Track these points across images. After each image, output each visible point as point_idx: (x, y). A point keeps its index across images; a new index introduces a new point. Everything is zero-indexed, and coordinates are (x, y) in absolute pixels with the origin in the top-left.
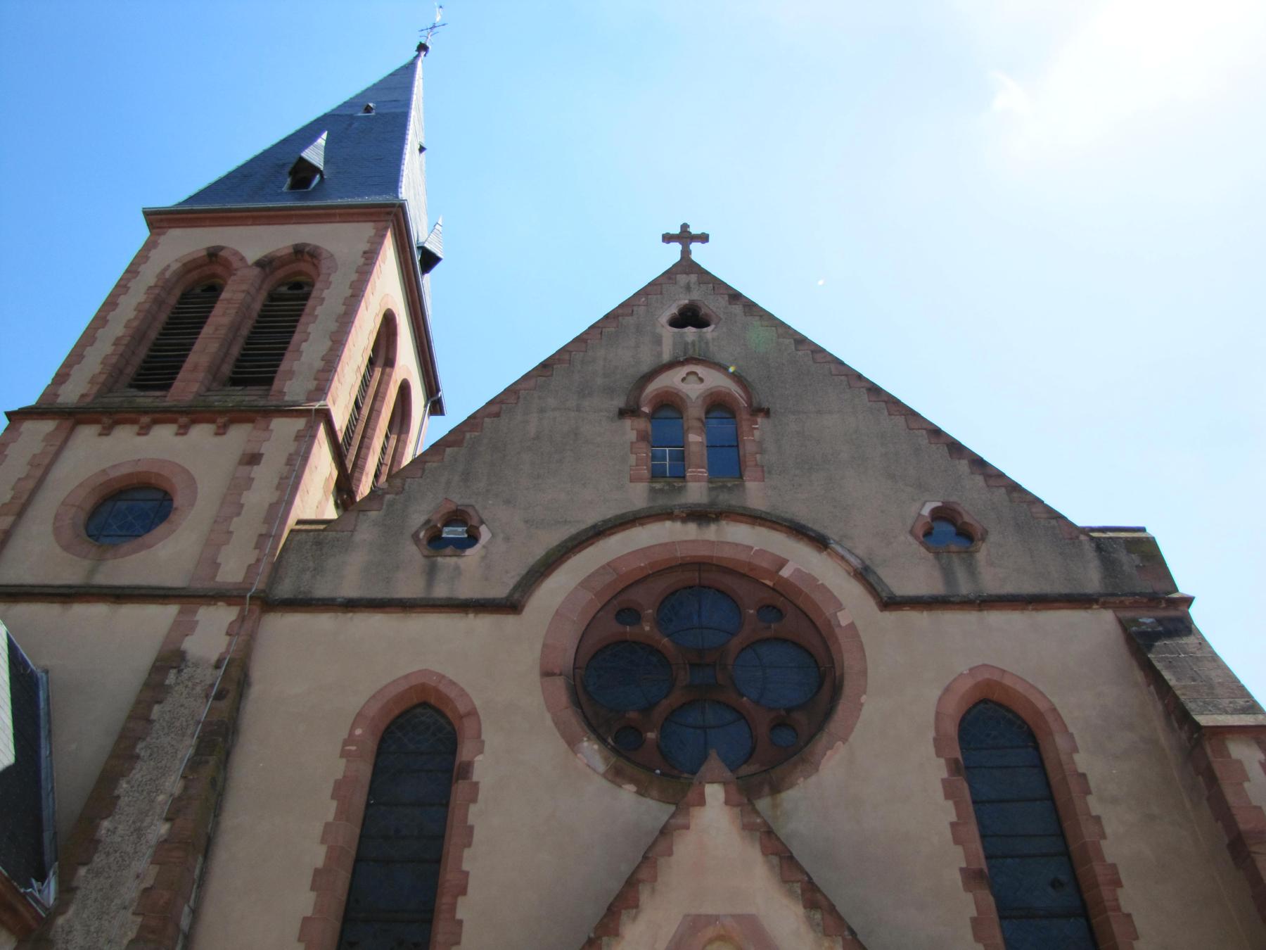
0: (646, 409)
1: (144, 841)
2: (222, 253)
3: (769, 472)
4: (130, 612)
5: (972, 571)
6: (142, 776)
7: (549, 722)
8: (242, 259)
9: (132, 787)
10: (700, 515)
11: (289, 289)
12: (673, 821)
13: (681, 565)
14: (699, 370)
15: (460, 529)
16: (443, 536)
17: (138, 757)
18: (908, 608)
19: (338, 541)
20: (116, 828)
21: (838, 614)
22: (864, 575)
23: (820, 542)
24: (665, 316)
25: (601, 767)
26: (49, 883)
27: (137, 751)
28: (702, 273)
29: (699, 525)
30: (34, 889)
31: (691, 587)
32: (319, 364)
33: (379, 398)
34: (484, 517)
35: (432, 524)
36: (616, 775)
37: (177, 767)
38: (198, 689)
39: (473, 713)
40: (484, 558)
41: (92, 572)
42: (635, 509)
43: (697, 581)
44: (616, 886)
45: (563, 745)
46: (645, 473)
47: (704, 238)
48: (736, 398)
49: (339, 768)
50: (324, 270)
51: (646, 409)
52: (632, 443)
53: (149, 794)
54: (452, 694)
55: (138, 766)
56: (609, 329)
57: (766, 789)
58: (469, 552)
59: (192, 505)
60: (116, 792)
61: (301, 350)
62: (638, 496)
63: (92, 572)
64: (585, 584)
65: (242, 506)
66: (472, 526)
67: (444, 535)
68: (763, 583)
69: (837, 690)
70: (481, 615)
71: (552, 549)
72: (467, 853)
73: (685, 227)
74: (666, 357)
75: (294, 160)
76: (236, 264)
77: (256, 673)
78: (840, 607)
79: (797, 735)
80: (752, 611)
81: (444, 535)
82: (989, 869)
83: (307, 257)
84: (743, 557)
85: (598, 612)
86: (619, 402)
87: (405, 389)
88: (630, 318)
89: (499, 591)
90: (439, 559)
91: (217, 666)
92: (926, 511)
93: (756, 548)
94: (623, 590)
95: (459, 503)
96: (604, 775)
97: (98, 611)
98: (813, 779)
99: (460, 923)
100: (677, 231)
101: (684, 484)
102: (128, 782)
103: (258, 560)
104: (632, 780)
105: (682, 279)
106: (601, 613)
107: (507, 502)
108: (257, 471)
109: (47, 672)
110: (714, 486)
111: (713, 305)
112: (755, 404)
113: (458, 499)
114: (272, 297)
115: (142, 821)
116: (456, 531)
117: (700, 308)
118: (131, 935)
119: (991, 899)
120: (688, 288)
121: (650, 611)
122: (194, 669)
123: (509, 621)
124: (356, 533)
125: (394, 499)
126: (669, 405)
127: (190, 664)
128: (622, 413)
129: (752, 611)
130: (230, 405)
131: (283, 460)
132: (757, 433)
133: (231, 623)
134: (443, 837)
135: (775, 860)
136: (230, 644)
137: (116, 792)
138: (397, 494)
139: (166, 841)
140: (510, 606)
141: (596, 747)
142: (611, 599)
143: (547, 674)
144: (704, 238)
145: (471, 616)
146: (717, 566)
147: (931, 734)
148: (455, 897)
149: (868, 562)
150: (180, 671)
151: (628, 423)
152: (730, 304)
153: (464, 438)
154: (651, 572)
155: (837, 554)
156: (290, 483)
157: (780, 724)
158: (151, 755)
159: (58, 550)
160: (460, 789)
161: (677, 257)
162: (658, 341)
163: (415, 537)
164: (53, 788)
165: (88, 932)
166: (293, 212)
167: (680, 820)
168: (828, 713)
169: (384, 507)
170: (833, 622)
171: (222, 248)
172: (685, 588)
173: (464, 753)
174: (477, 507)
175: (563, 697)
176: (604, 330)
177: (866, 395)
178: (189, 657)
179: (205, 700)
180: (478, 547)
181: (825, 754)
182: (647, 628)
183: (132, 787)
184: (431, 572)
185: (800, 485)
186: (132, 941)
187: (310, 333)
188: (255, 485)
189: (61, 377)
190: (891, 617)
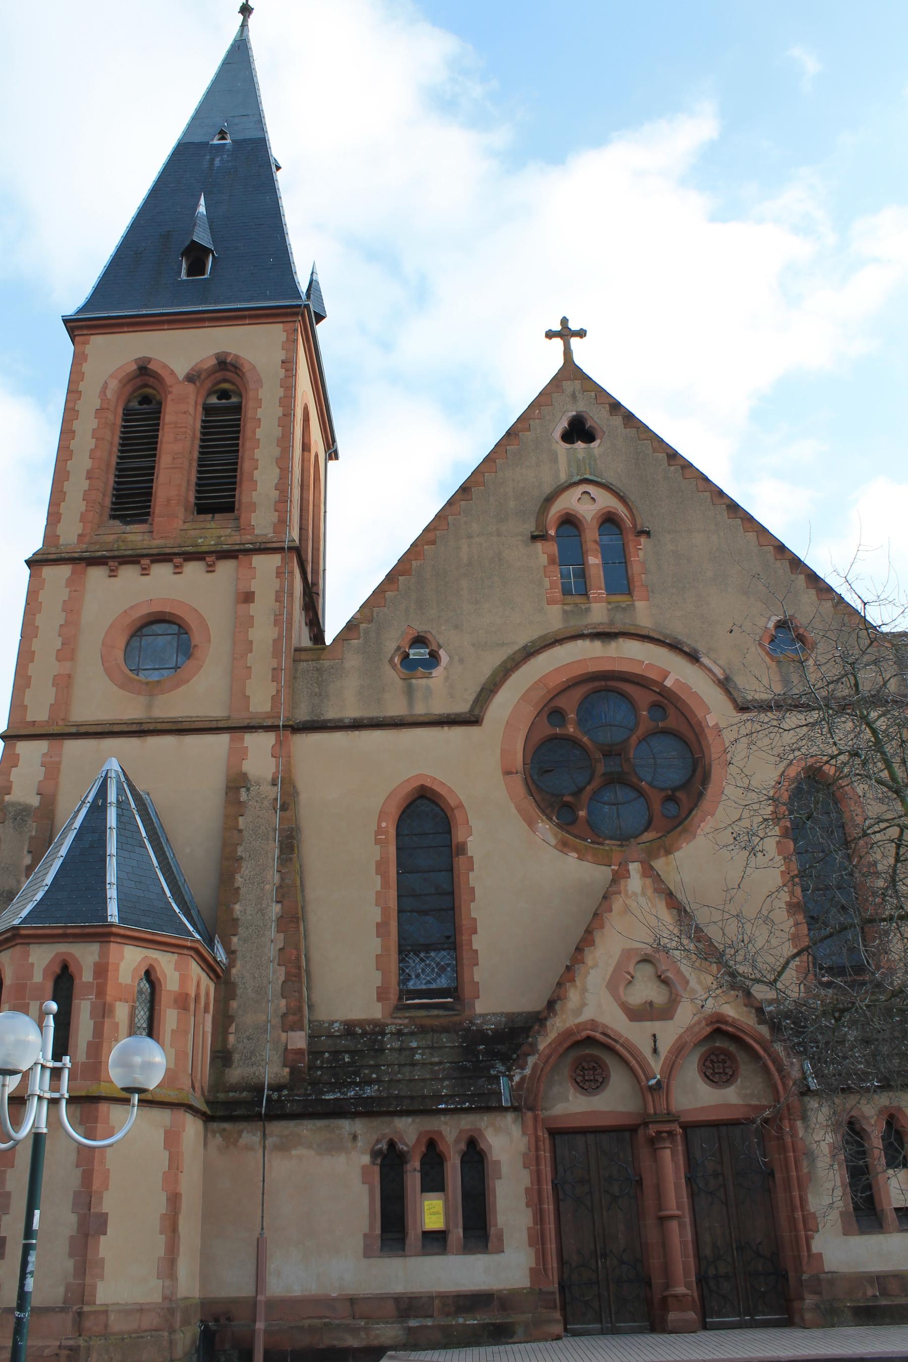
0: (552, 532)
1: (267, 918)
2: (149, 366)
3: (653, 592)
4: (191, 740)
6: (250, 872)
7: (514, 811)
8: (172, 373)
9: (246, 880)
11: (219, 398)
12: (610, 889)
14: (590, 488)
15: (422, 651)
17: (241, 858)
19: (332, 668)
20: (245, 910)
21: (707, 716)
22: (725, 684)
23: (693, 657)
24: (557, 434)
25: (553, 842)
26: (217, 948)
27: (239, 854)
28: (584, 379)
29: (603, 642)
30: (762, 1160)
32: (275, 494)
33: (305, 487)
34: (441, 642)
35: (402, 650)
36: (564, 846)
37: (271, 864)
38: (266, 803)
39: (460, 806)
40: (447, 678)
41: (149, 706)
42: (554, 630)
44: (580, 932)
45: (527, 827)
46: (558, 593)
47: (581, 334)
48: (623, 520)
49: (376, 852)
50: (251, 385)
51: (552, 532)
52: (545, 567)
53: (258, 884)
54: (443, 792)
55: (244, 864)
56: (512, 447)
57: (662, 852)
59: (209, 641)
60: (236, 885)
61: (254, 479)
63: (149, 706)
64: (525, 698)
65: (251, 642)
66: (432, 650)
69: (706, 778)
71: (496, 668)
72: (473, 905)
73: (564, 321)
74: (563, 477)
75: (187, 243)
76: (168, 380)
77: (301, 785)
78: (708, 711)
81: (411, 657)
82: (803, 897)
83: (233, 369)
84: (637, 670)
85: (535, 718)
86: (530, 527)
87: (317, 456)
88: (529, 433)
89: (462, 707)
90: (414, 681)
91: (274, 784)
92: (771, 625)
93: (646, 662)
94: (551, 699)
95: (419, 630)
96: (555, 847)
97: (169, 741)
98: (692, 844)
99: (476, 951)
100: (557, 327)
101: (588, 605)
102: (241, 877)
103: (278, 691)
104: (575, 850)
105: (569, 386)
106: (537, 718)
107: (456, 627)
108: (253, 609)
109: (148, 794)
111: (597, 417)
112: (639, 528)
113: (419, 627)
114: (208, 410)
115: (261, 904)
117: (586, 419)
118: (282, 978)
121: (572, 716)
122: (258, 787)
123: (473, 730)
124: (345, 661)
125: (368, 628)
126: (569, 521)
127: (253, 783)
128: (534, 538)
129: (644, 713)
130: (213, 543)
131: (273, 597)
132: (641, 553)
133: (273, 747)
135: (675, 912)
136: (277, 765)
137: (236, 885)
138: (369, 623)
139: (282, 916)
140: (471, 720)
141: (547, 826)
143: (507, 773)
144: (581, 334)
145: (446, 728)
148: (470, 935)
149: (728, 671)
150: (248, 790)
151: (539, 545)
152: (611, 415)
153: (411, 565)
155: (705, 667)
157: (671, 798)
158: (250, 856)
159: (115, 688)
160: (460, 862)
161: (559, 362)
162: (554, 459)
163: (391, 661)
164: (185, 880)
165: (255, 977)
166: (206, 315)
167: (613, 889)
168: (700, 795)
169: (362, 635)
170: (704, 724)
171: (149, 360)
172: (594, 692)
173: (459, 835)
174: (433, 632)
175: (521, 789)
176: (508, 447)
177: (726, 513)
178: (250, 777)
179: (273, 811)
181: (699, 826)
182: (571, 730)
183: (246, 880)
184: (410, 692)
185: (677, 603)
186: (284, 982)
187: (258, 460)
188: (256, 622)
189: (54, 517)
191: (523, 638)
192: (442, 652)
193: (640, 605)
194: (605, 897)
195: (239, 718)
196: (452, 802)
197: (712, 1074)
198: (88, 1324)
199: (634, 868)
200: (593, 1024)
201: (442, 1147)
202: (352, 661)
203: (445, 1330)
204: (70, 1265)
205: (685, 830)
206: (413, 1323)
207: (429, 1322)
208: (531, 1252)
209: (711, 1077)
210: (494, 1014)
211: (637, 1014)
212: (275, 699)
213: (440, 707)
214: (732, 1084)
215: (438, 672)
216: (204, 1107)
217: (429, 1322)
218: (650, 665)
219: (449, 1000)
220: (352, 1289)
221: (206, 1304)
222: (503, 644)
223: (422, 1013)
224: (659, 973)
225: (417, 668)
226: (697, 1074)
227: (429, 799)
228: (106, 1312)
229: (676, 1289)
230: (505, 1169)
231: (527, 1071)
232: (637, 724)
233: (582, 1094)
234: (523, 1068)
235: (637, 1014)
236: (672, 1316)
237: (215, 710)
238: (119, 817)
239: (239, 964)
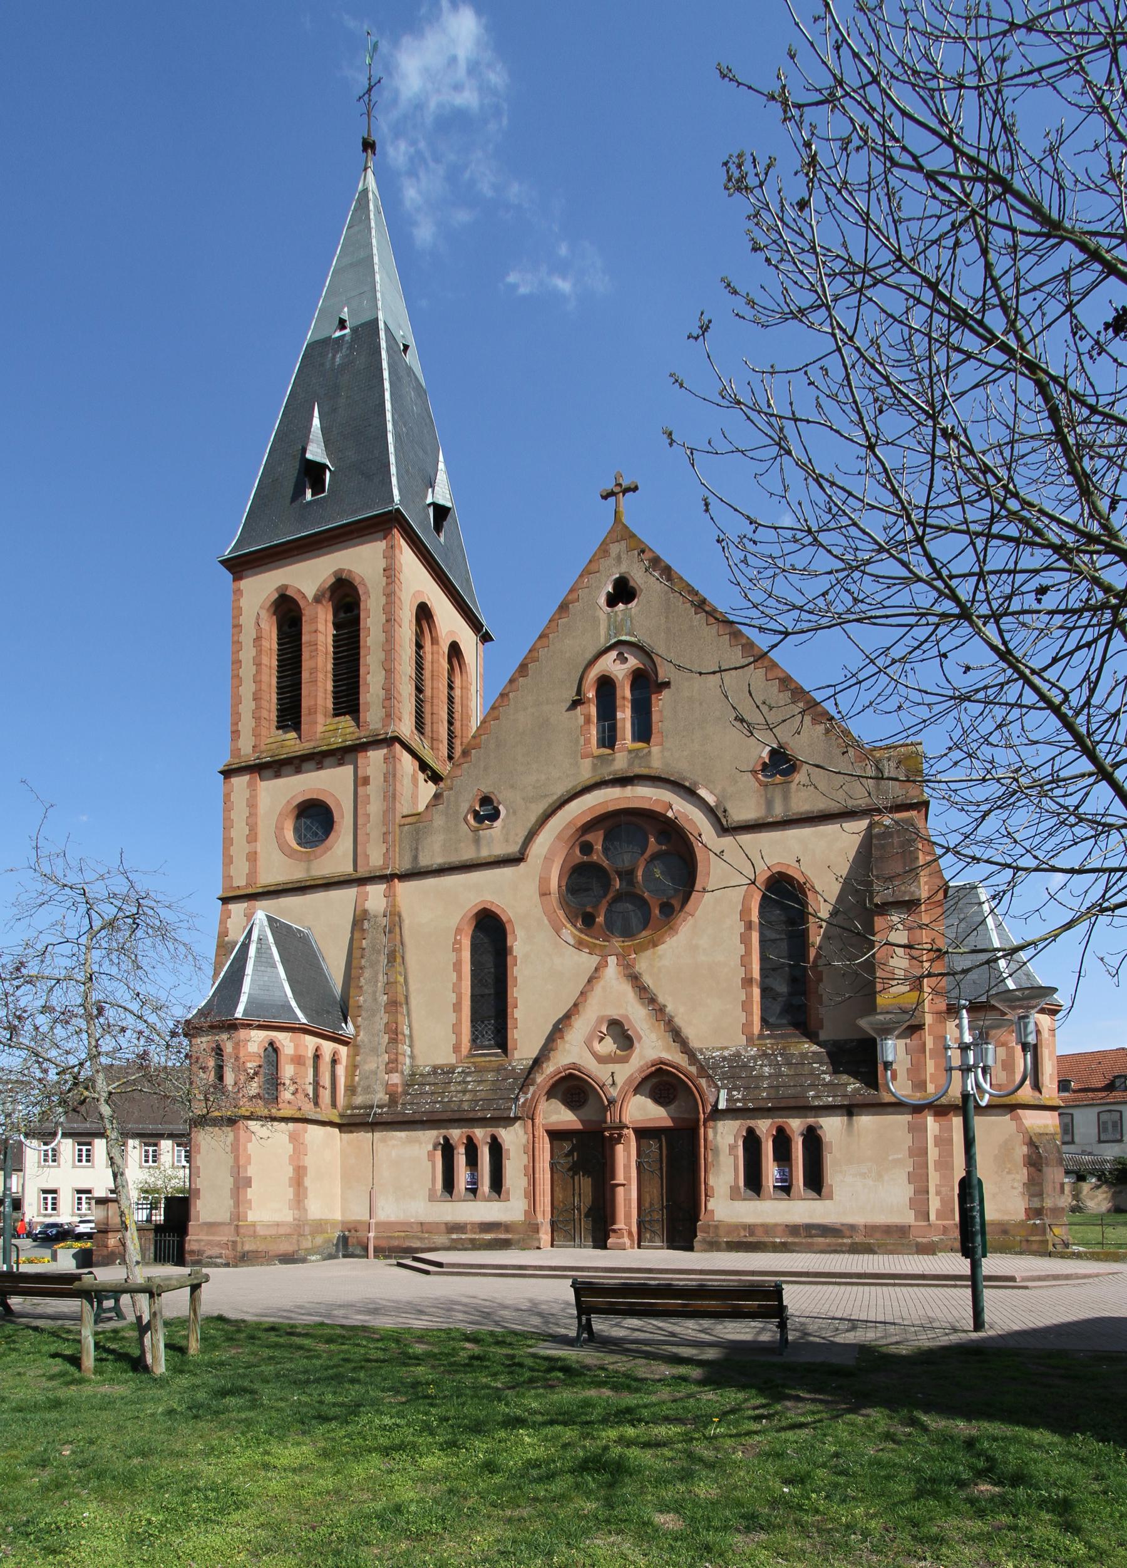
2: (288, 593)
5: (786, 798)
7: (546, 922)
10: (623, 781)
11: (345, 613)
22: (710, 812)
24: (602, 600)
36: (580, 945)
39: (510, 921)
40: (503, 827)
41: (308, 870)
54: (498, 912)
62: (586, 773)
63: (308, 870)
64: (559, 837)
65: (369, 815)
76: (302, 604)
84: (646, 806)
89: (513, 849)
107: (512, 787)
113: (485, 789)
120: (619, 558)
147: (740, 908)
156: (390, 796)
171: (286, 587)
180: (500, 820)
184: (477, 841)
191: (560, 790)
192: (501, 808)
193: (655, 750)
194: (589, 981)
195: (362, 872)
198: (242, 1231)
199: (612, 960)
200: (574, 1066)
201: (758, 1132)
202: (439, 821)
203: (472, 1240)
204: (231, 1202)
205: (671, 928)
206: (454, 1236)
207: (463, 1236)
208: (526, 1201)
211: (602, 1059)
212: (386, 855)
213: (500, 849)
215: (498, 824)
216: (337, 1120)
217: (463, 1236)
220: (423, 1219)
221: (343, 1223)
223: (483, 1059)
228: (254, 1226)
230: (512, 1154)
231: (529, 1096)
234: (526, 1093)
235: (602, 1059)
237: (345, 868)
238: (258, 950)
239: (362, 1034)
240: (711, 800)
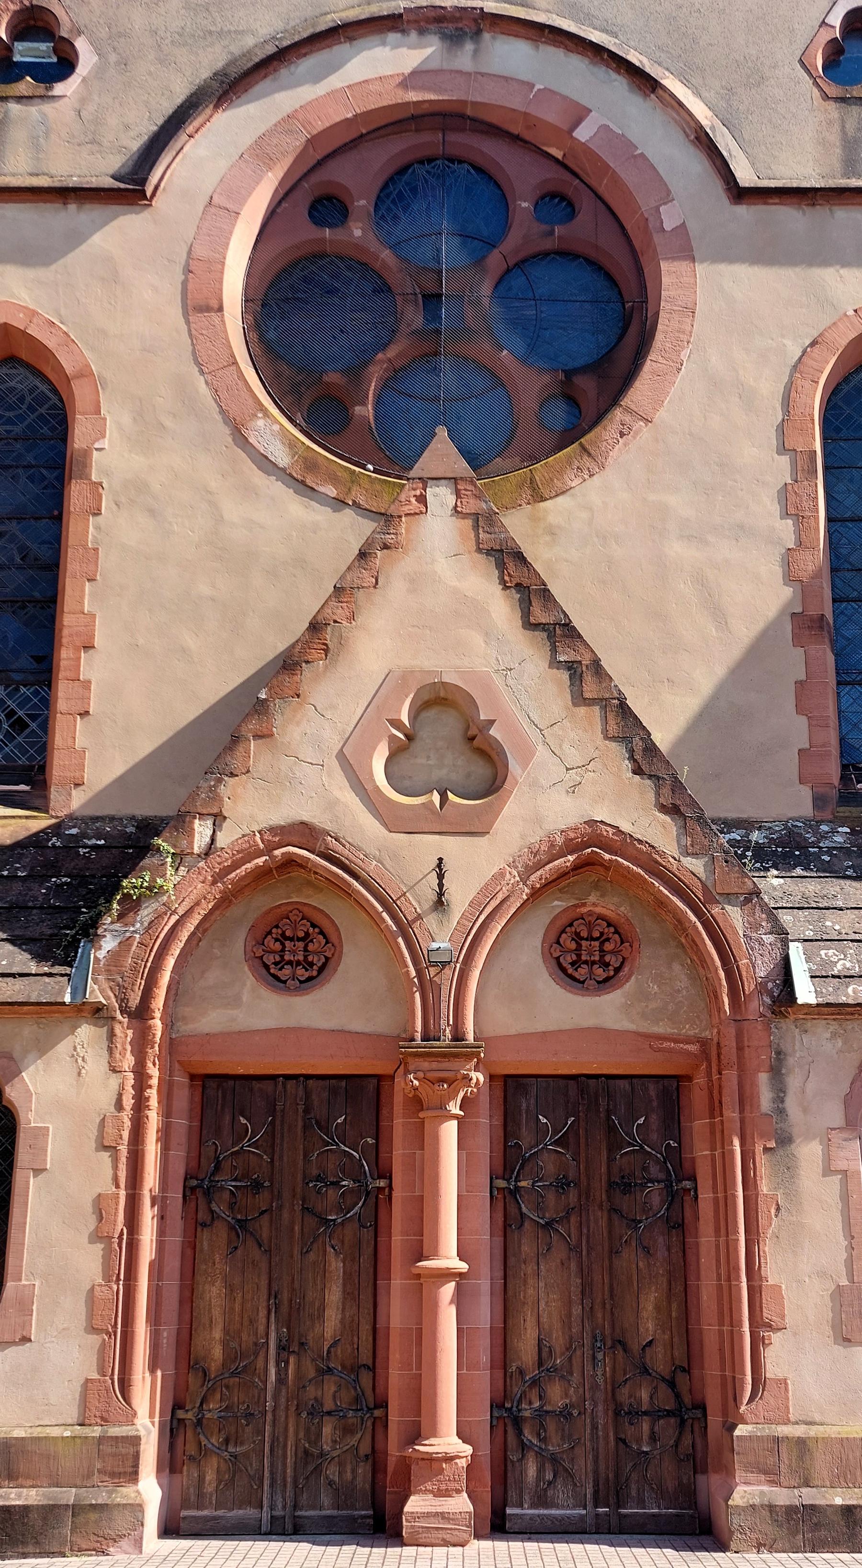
13: (413, 117)
16: (15, 59)
18: (777, 201)
31: (430, 160)
43: (441, 152)
58: (59, 88)
67: (17, 58)
68: (547, 153)
70: (88, 206)
78: (667, 197)
79: (580, 412)
80: (525, 205)
84: (515, 103)
92: (836, 19)
93: (538, 86)
94: (320, 164)
106: (284, 205)
110: (273, 1310)
116: (38, 49)
119: (831, 658)
121: (363, 202)
129: (525, 205)
134: (57, 565)
142: (300, 180)
145: (72, 207)
146: (473, 120)
154: (364, 131)
182: (358, 233)
190: (742, 210)
192: (81, 44)
196: (68, 365)
197: (573, 964)
209: (570, 971)
210: (112, 819)
214: (615, 988)
218: (547, 92)
219: (22, 787)
222: (220, 34)
224: (473, 731)
225: (23, 78)
226: (540, 960)
227: (28, 366)
229: (432, 1441)
232: (505, 226)
233: (274, 989)
236: (415, 1504)
240: (560, 157)
